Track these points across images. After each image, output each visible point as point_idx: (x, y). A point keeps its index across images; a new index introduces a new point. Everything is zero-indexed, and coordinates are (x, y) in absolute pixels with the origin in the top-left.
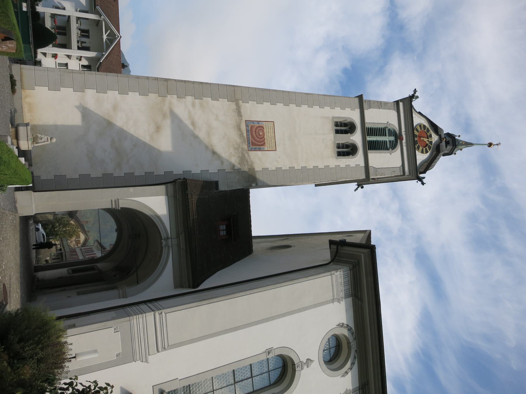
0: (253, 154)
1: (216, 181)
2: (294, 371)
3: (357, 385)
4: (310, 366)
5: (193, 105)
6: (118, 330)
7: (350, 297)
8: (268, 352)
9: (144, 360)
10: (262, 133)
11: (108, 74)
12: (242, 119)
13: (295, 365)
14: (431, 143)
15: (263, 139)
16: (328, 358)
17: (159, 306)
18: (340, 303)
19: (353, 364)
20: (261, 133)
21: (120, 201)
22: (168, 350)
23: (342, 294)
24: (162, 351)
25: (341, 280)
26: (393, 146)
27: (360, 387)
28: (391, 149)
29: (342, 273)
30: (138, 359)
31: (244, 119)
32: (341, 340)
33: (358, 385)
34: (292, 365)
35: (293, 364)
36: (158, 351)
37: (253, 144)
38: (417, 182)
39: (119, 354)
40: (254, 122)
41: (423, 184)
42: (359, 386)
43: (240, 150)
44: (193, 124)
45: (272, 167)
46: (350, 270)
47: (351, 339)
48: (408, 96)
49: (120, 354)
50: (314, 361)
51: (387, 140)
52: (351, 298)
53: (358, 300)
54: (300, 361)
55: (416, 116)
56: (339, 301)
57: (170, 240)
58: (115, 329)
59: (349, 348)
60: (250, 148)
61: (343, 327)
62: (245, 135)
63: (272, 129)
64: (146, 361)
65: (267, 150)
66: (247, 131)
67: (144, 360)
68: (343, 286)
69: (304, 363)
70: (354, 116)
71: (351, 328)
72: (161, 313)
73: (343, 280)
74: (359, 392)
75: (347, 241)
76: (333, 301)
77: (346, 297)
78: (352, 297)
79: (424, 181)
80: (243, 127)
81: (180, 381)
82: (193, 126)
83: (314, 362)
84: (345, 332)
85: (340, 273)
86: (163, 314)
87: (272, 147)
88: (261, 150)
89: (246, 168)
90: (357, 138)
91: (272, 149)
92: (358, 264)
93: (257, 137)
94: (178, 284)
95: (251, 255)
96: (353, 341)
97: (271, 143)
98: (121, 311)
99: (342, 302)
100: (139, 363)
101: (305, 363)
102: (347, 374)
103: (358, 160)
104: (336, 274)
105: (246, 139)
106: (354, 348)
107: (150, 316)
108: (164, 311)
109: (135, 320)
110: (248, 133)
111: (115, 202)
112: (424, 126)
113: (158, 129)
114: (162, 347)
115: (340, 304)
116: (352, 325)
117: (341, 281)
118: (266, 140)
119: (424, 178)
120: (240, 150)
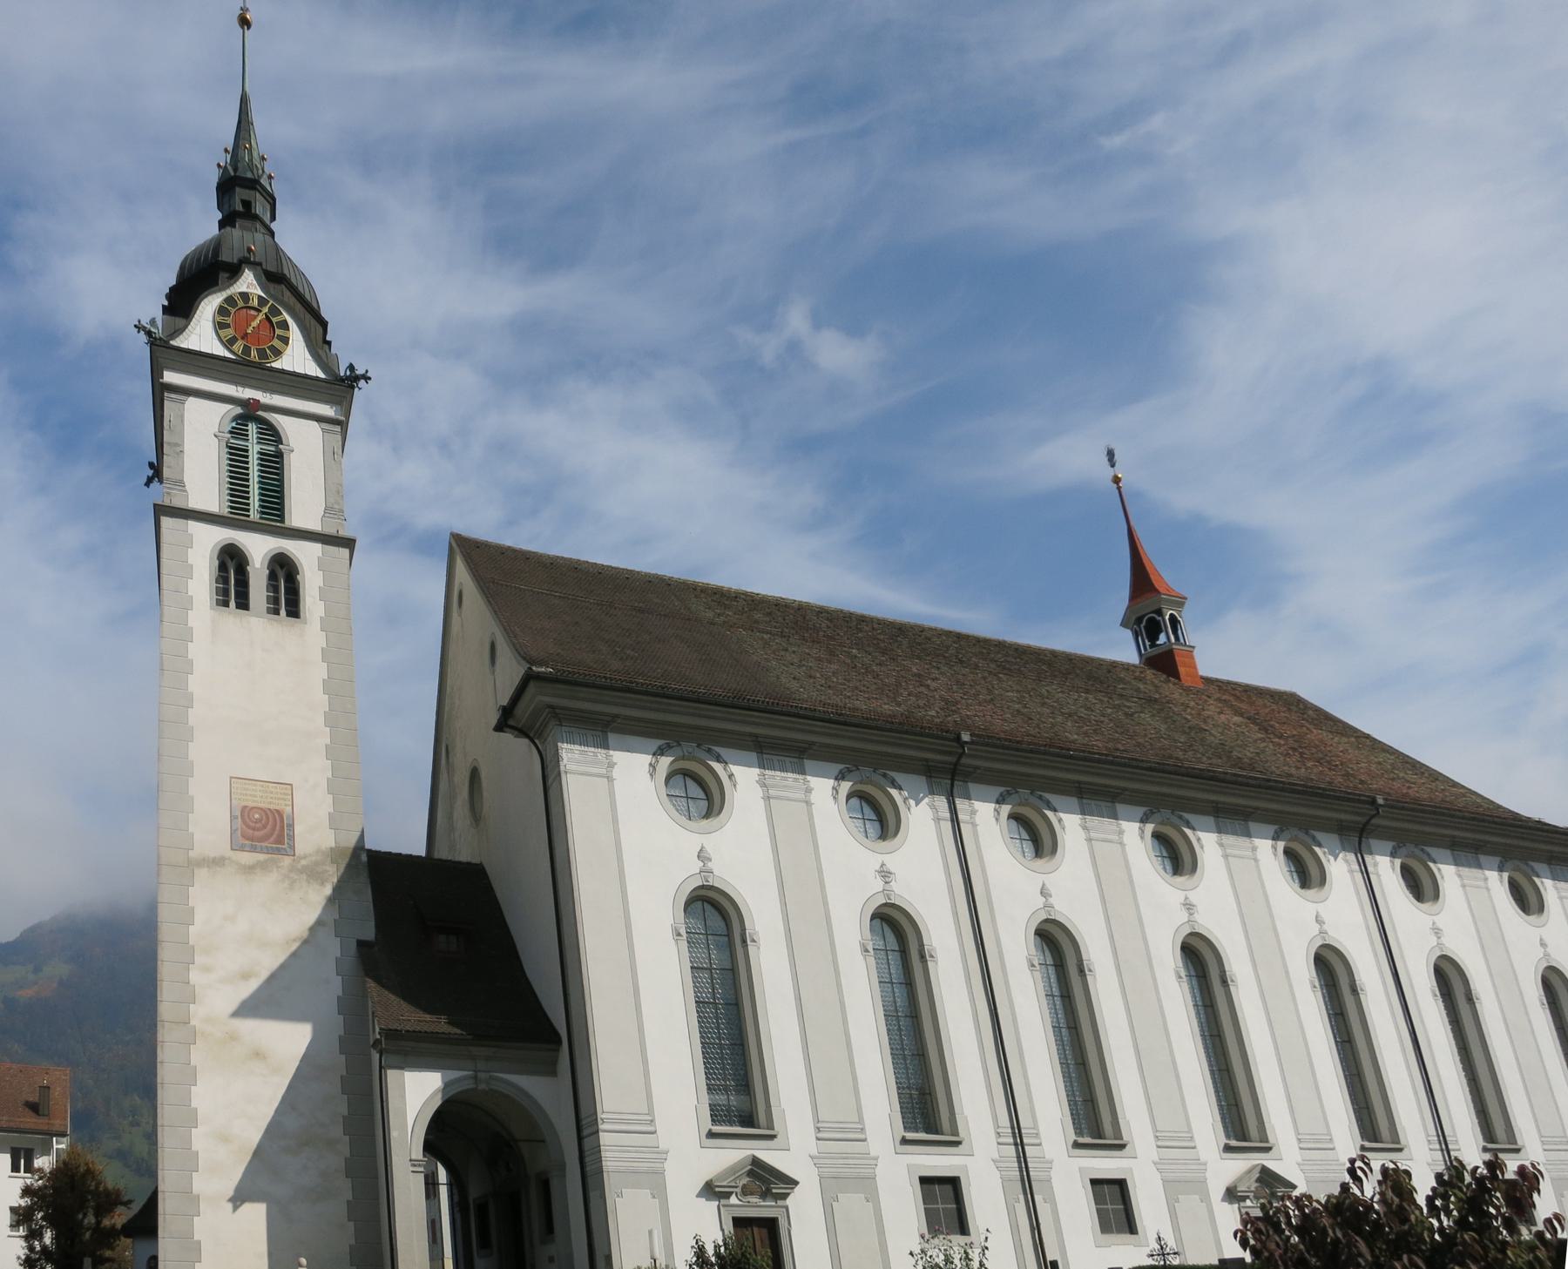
0: (301, 847)
1: (358, 945)
2: (712, 888)
3: (753, 756)
5: (207, 969)
8: (677, 936)
10: (256, 812)
11: (159, 1145)
12: (229, 859)
14: (262, 301)
15: (268, 812)
16: (873, 829)
17: (589, 1120)
18: (616, 764)
19: (719, 759)
20: (257, 816)
21: (413, 1157)
23: (601, 752)
26: (271, 434)
28: (281, 446)
31: (229, 853)
33: (924, 778)
35: (702, 887)
36: (654, 1133)
37: (280, 840)
38: (360, 389)
39: (652, 1194)
40: (233, 828)
41: (367, 378)
43: (292, 875)
44: (246, 976)
45: (326, 805)
46: (562, 725)
47: (678, 751)
48: (149, 348)
51: (257, 448)
55: (195, 332)
56: (611, 765)
57: (479, 1074)
58: (618, 1196)
59: (694, 759)
60: (288, 849)
62: (262, 857)
63: (245, 784)
65: (291, 807)
66: (253, 849)
67: (874, 1162)
70: (206, 541)
71: (660, 748)
72: (602, 1119)
75: (505, 704)
76: (610, 779)
79: (360, 371)
80: (247, 858)
82: (250, 977)
84: (665, 762)
85: (564, 750)
86: (603, 1116)
87: (285, 794)
88: (291, 823)
89: (333, 874)
90: (259, 548)
91: (287, 794)
93: (264, 827)
94: (551, 1070)
95: (485, 866)
97: (277, 793)
98: (590, 1181)
99: (615, 760)
102: (733, 774)
103: (306, 555)
104: (565, 761)
105: (270, 855)
107: (605, 1139)
108: (600, 1116)
109: (609, 1163)
110: (259, 850)
111: (415, 1165)
112: (222, 311)
113: (258, 1055)
116: (656, 743)
118: (272, 807)
119: (351, 367)
120: (296, 877)
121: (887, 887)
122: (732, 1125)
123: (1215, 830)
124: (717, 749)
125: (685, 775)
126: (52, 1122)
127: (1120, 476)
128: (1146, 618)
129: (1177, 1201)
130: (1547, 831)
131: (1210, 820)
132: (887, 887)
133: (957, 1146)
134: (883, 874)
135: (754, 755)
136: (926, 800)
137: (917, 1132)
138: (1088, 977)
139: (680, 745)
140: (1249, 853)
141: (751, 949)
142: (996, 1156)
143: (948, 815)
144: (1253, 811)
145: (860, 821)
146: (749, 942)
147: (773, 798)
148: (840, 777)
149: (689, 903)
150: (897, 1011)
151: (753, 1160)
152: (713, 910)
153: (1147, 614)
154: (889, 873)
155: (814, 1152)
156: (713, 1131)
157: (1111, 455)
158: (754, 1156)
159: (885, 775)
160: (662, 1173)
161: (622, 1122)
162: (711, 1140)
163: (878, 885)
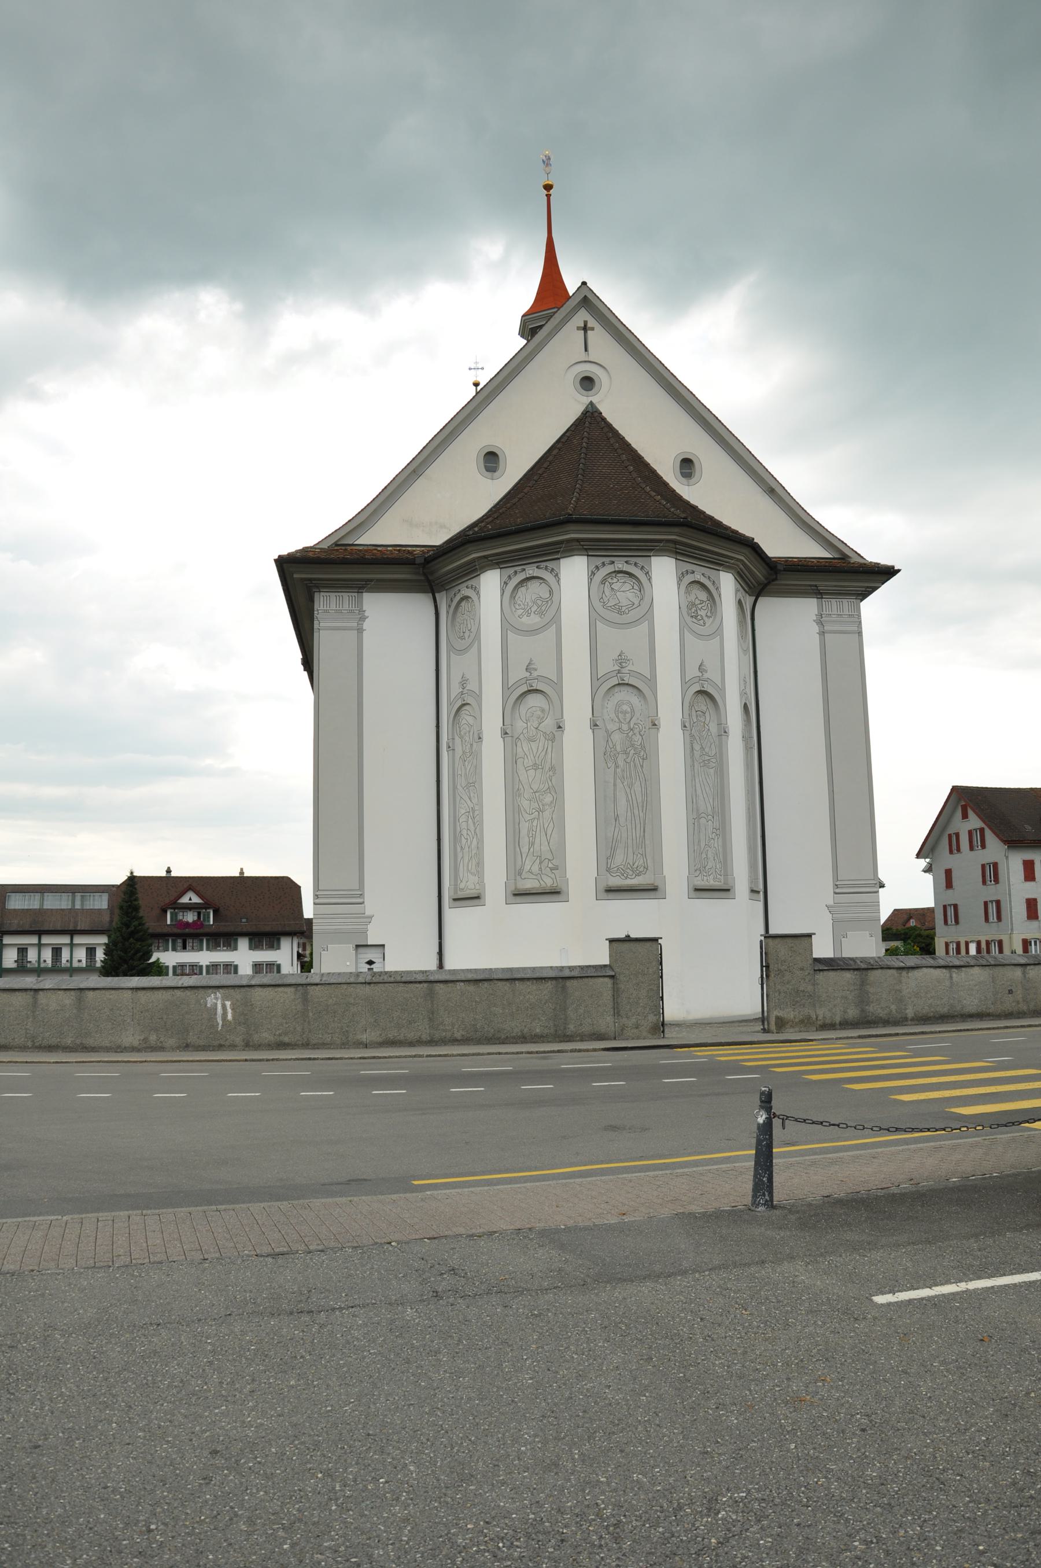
58: (324, 950)
126: (838, 1022)
155: (831, 903)
157: (547, 162)
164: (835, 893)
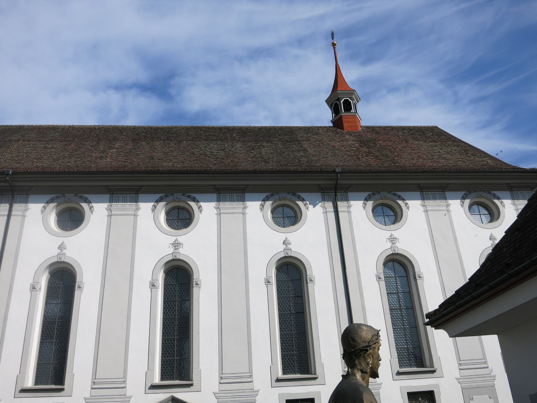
2: (397, 254)
4: (290, 241)
6: (471, 397)
7: (445, 193)
9: (379, 386)
13: (285, 256)
16: (486, 218)
22: (252, 374)
24: (488, 364)
25: (119, 205)
27: (510, 190)
29: (113, 203)
30: (492, 383)
32: (168, 210)
33: (509, 192)
34: (285, 258)
39: (489, 397)
42: (510, 191)
49: (489, 396)
50: (491, 234)
52: (446, 192)
53: (142, 189)
54: (57, 256)
58: (471, 400)
61: (264, 205)
64: (258, 391)
67: (379, 386)
68: (126, 204)
69: (286, 247)
71: (267, 197)
73: (121, 202)
74: (425, 191)
77: (445, 198)
78: (245, 193)
81: (392, 358)
83: (64, 242)
92: (214, 186)
96: (381, 194)
99: (140, 206)
100: (495, 382)
101: (286, 246)
106: (286, 195)
114: (249, 378)
115: (142, 208)
117: (120, 205)
121: (394, 245)
122: (411, 367)
123: (511, 198)
124: (193, 195)
125: (478, 205)
127: (335, 42)
128: (334, 103)
129: (472, 399)
130: (518, 172)
131: (508, 193)
132: (176, 251)
133: (433, 373)
134: (392, 240)
135: (419, 193)
136: (320, 204)
137: (296, 374)
138: (418, 281)
139: (65, 196)
140: (445, 208)
141: (419, 281)
142: (458, 376)
143: (332, 210)
144: (139, 187)
145: (478, 216)
146: (417, 278)
147: (328, 212)
148: (463, 198)
149: (385, 264)
150: (400, 306)
151: (172, 398)
152: (398, 265)
153: (333, 103)
154: (395, 239)
155: (217, 390)
156: (400, 372)
158: (172, 396)
159: (395, 194)
160: (493, 386)
161: (107, 383)
162: (150, 390)
163: (389, 245)
164: (220, 383)
